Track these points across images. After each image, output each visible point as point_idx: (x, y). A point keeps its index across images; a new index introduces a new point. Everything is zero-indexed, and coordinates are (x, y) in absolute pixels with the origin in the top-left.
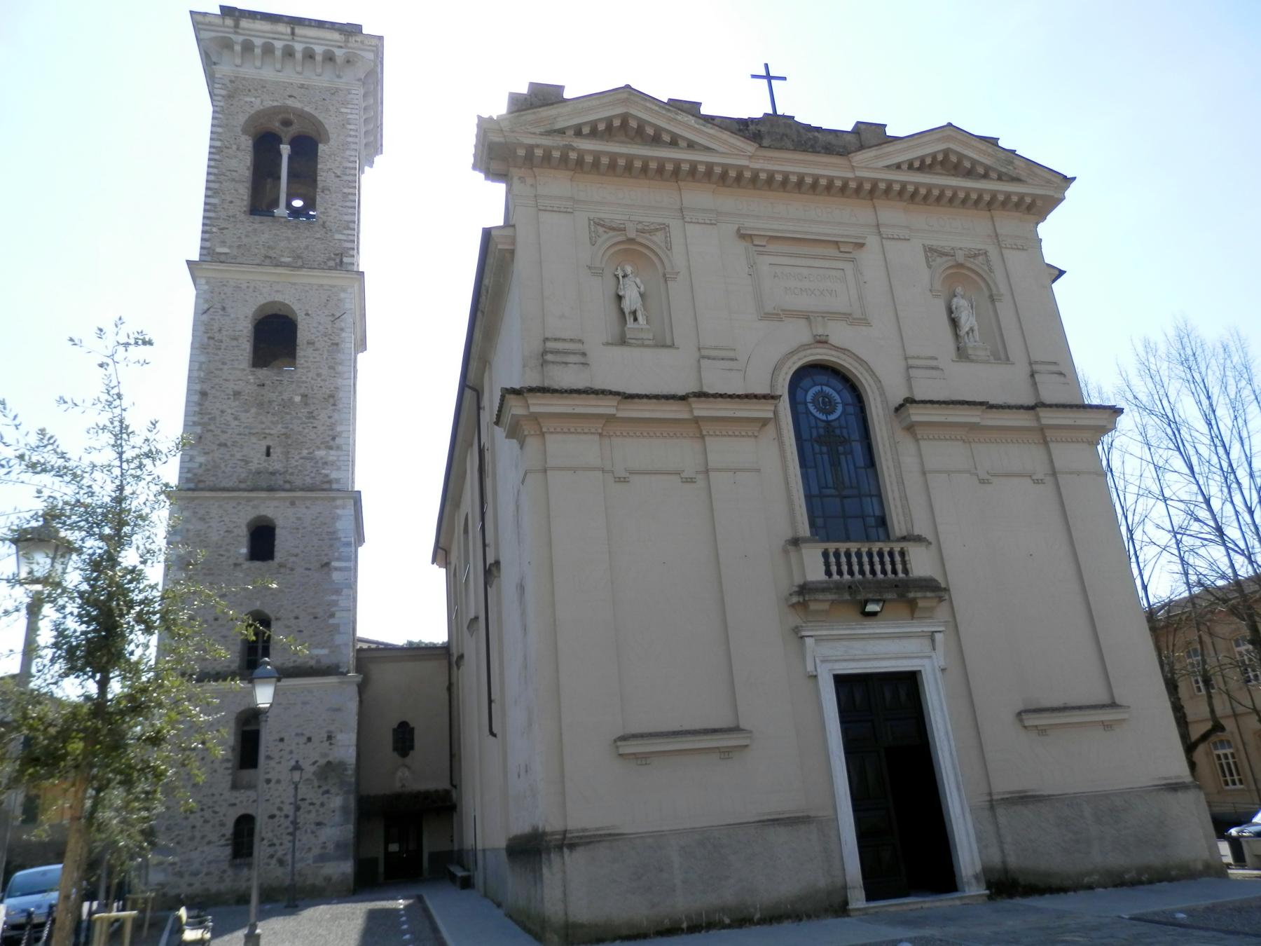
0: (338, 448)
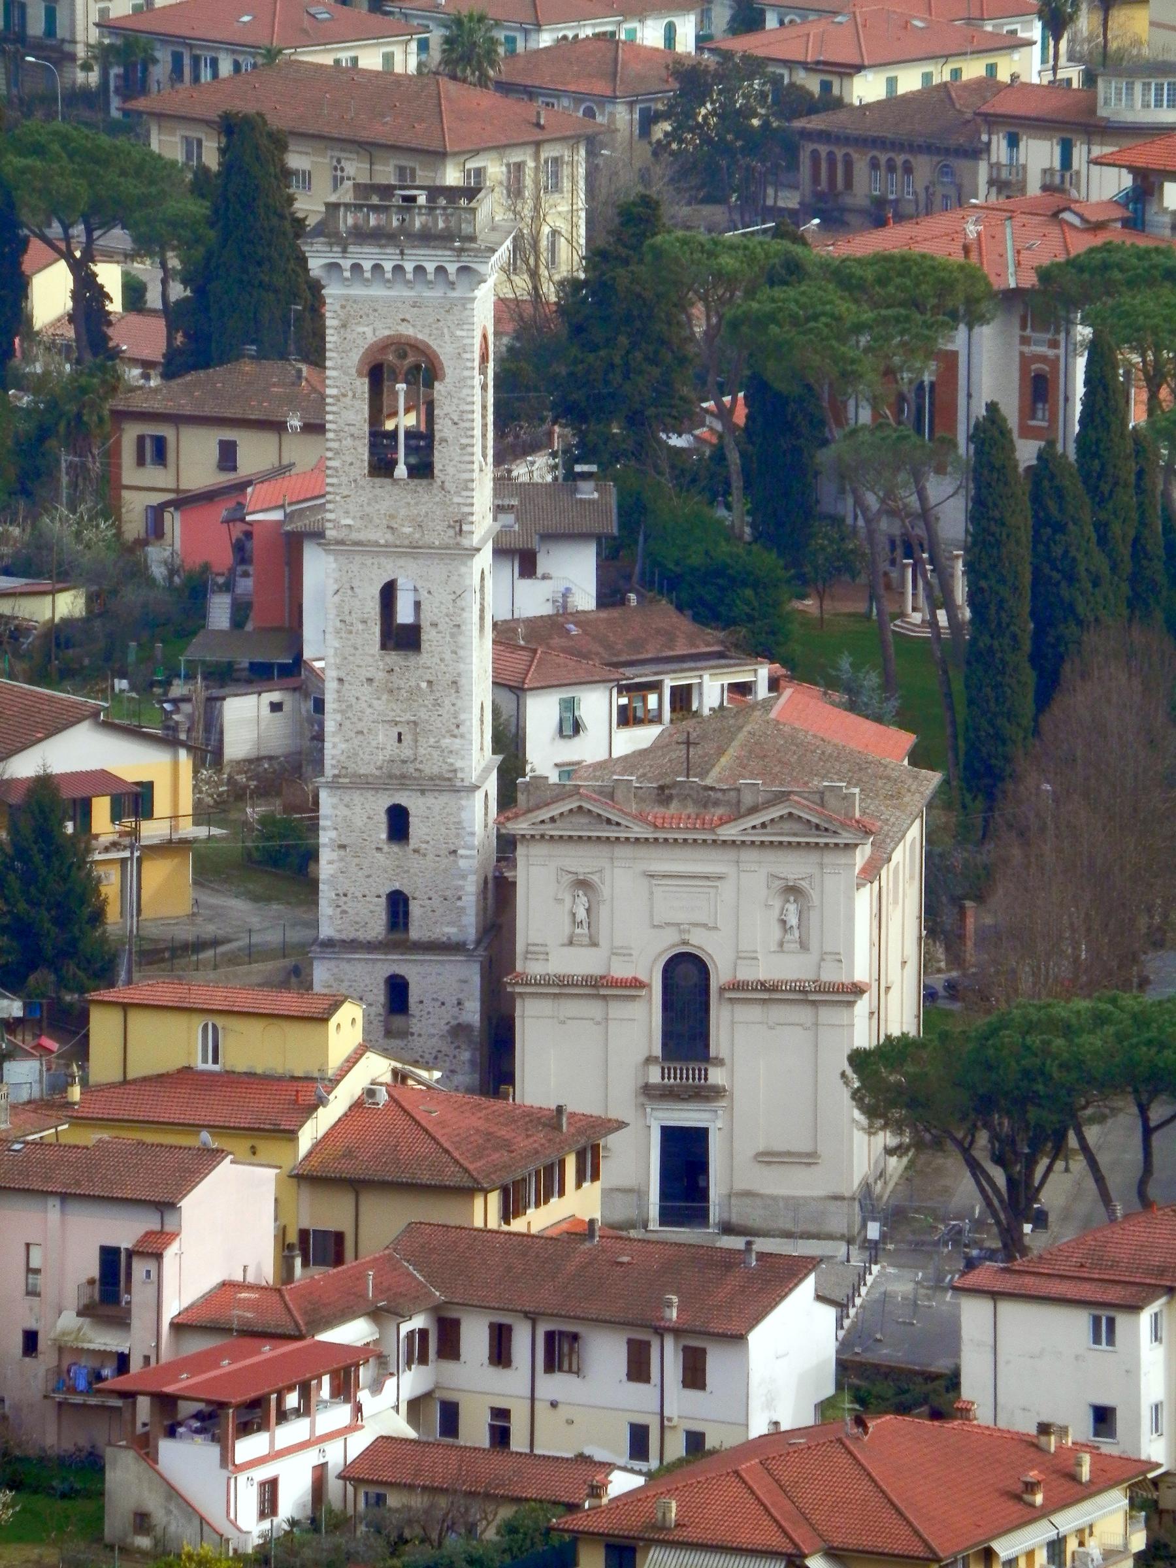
0: (462, 736)
